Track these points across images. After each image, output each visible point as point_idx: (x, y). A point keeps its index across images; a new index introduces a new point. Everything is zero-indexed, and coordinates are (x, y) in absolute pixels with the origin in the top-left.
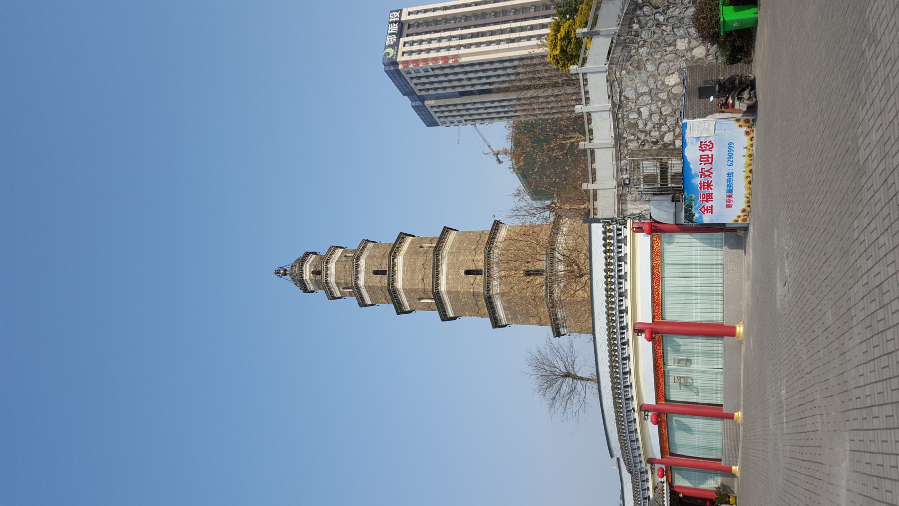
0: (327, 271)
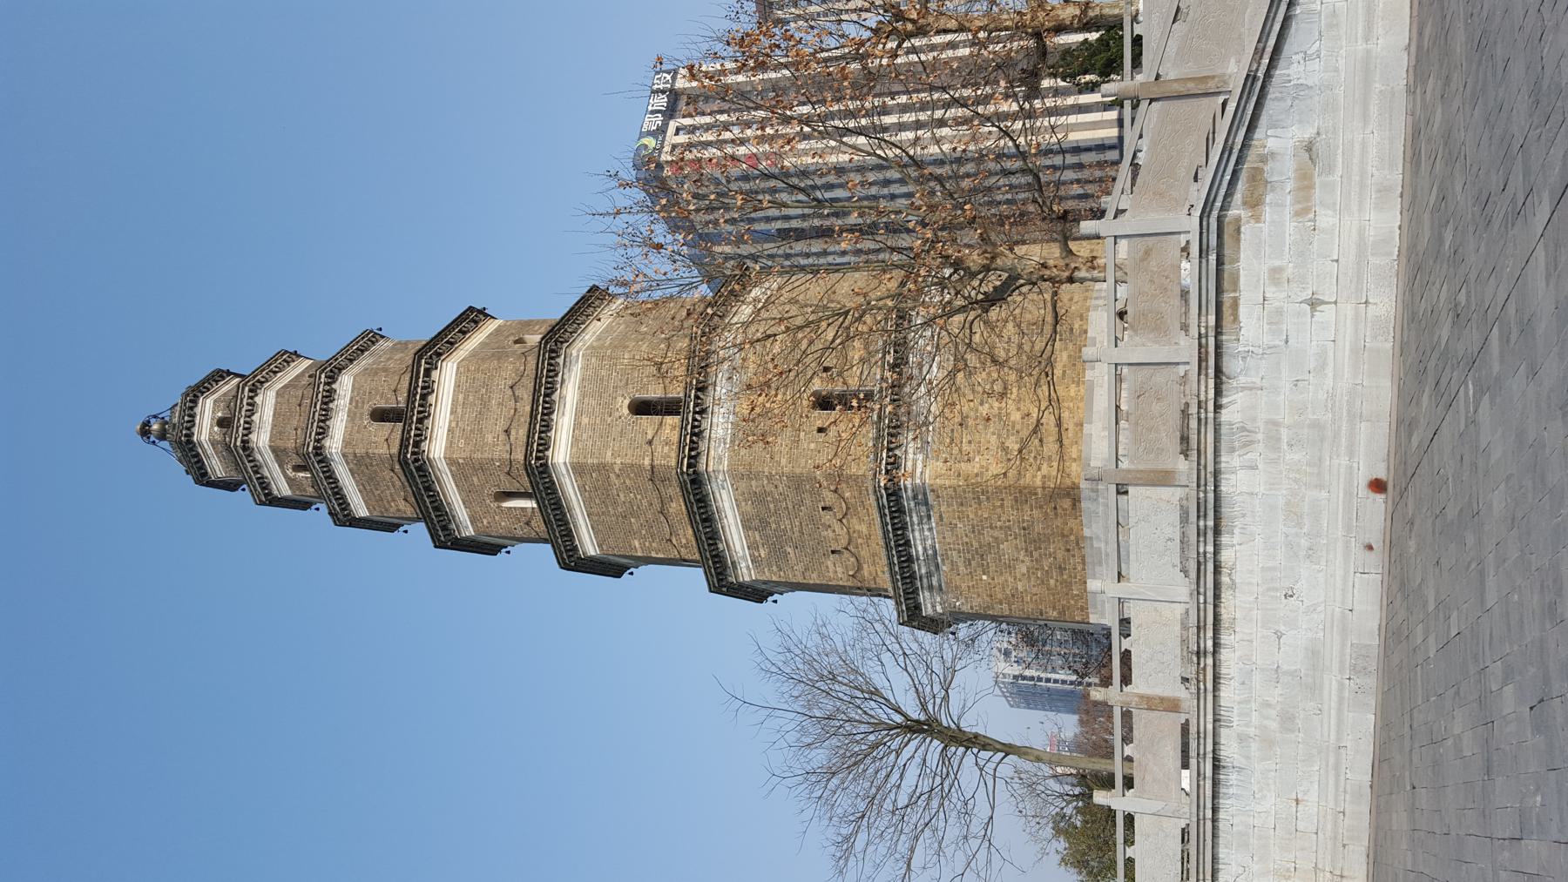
0: (251, 413)
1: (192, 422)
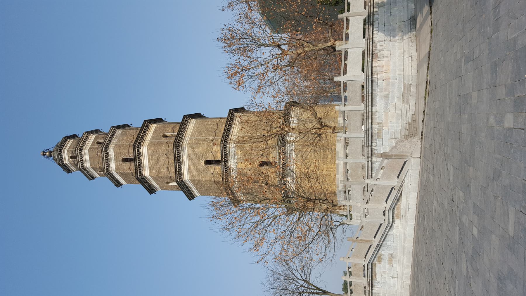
0: (82, 158)
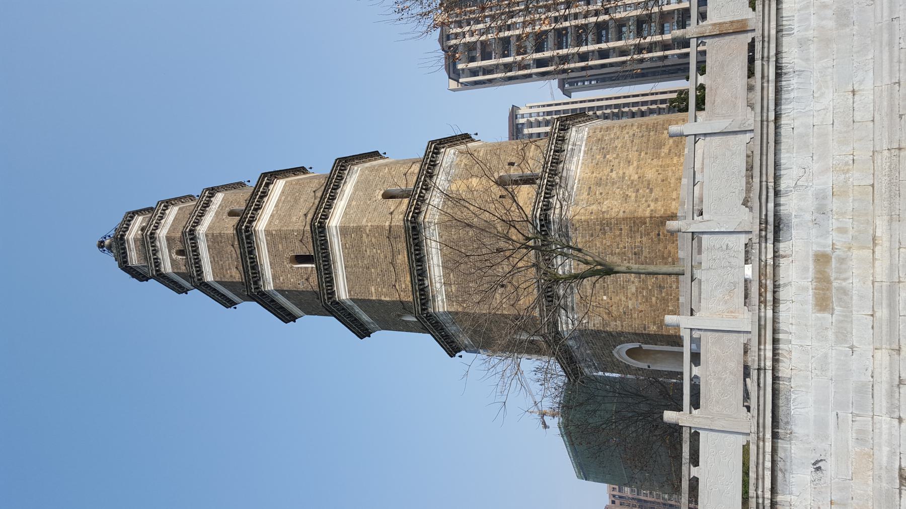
0: (162, 218)
1: (127, 228)
